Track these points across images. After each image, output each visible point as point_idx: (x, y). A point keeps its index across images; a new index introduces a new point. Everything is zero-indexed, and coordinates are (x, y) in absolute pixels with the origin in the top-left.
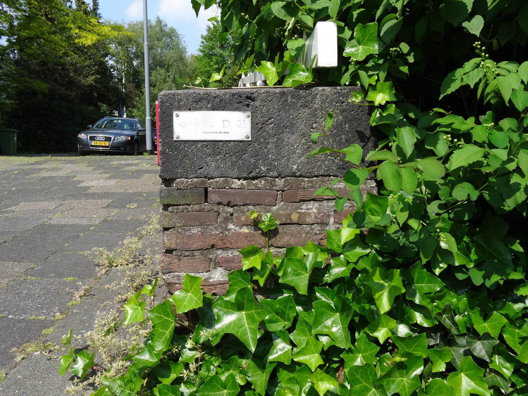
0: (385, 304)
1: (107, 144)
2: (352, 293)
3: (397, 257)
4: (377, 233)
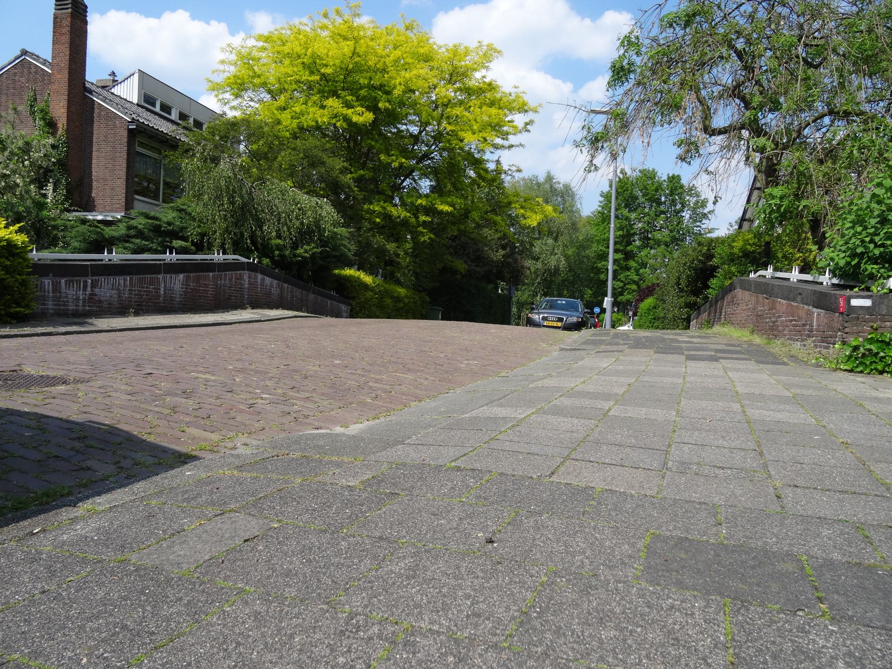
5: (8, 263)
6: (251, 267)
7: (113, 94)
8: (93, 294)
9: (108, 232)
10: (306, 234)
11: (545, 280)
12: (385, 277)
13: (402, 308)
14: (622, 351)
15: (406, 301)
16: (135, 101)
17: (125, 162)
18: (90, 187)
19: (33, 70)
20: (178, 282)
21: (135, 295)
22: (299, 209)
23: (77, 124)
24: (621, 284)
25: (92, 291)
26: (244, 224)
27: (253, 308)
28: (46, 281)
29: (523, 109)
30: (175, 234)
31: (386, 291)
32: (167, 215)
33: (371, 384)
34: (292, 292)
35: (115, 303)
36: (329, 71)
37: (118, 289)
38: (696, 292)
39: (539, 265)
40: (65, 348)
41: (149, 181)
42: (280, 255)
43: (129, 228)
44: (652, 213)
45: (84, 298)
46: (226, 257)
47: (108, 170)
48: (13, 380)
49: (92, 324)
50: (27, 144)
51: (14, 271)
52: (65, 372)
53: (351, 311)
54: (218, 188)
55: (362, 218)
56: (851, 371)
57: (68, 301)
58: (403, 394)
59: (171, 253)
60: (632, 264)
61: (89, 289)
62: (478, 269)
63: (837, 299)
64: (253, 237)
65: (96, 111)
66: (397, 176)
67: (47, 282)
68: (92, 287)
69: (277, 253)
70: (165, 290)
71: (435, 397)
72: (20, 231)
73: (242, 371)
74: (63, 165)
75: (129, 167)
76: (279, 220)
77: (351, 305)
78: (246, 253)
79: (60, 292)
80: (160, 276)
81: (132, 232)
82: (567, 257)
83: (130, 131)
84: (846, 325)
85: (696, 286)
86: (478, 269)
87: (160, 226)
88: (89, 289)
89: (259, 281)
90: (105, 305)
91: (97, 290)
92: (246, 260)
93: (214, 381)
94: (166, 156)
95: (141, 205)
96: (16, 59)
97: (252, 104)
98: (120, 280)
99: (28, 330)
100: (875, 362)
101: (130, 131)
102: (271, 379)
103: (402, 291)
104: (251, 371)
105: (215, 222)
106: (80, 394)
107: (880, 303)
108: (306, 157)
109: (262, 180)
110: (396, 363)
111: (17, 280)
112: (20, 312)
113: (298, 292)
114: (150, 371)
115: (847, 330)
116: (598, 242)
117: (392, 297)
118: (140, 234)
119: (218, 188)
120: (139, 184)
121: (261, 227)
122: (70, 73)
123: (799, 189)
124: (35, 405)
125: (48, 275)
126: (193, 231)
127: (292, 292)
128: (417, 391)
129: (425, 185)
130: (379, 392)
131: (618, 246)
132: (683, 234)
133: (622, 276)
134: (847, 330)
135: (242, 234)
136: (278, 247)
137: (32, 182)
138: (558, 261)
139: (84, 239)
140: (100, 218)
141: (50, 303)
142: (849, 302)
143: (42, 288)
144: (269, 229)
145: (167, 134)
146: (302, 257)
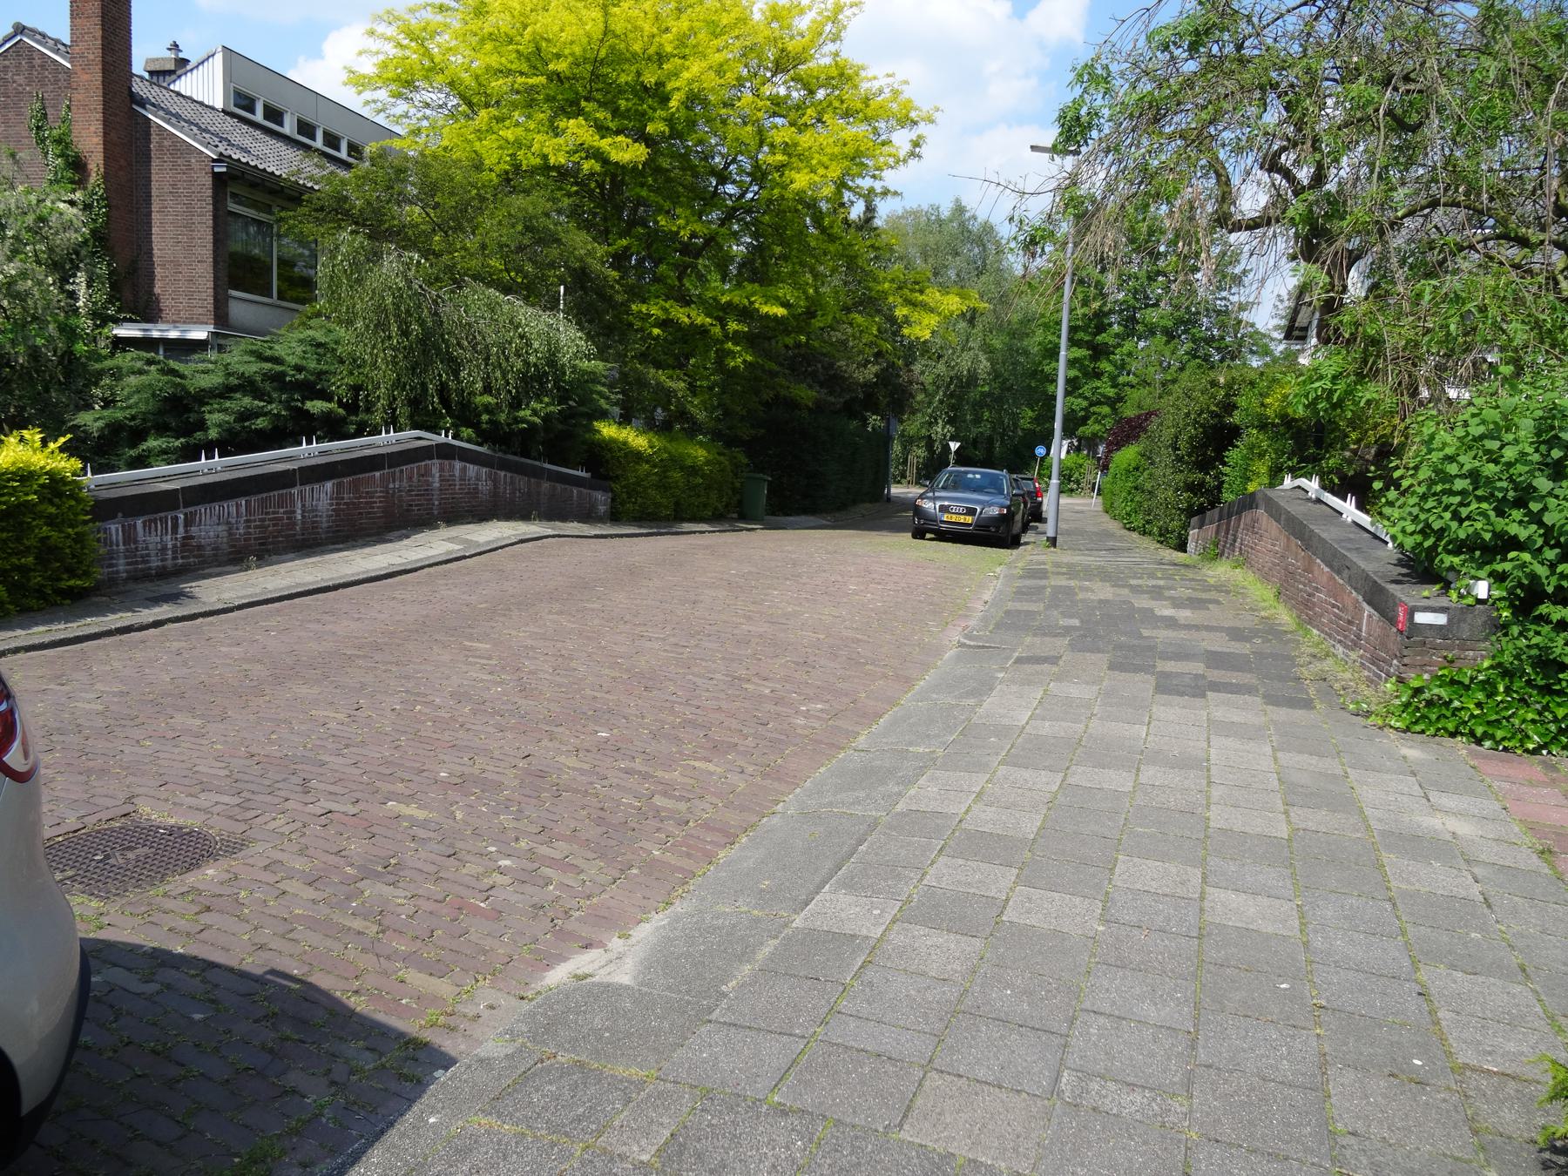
0: (1501, 689)
1: (969, 519)
2: (1489, 687)
3: (1507, 673)
4: (1500, 665)
5: (53, 510)
6: (445, 452)
7: (178, 94)
10: (532, 382)
11: (952, 395)
14: (1054, 660)
16: (219, 105)
17: (210, 232)
19: (37, 62)
20: (323, 497)
22: (522, 337)
23: (122, 162)
24: (1085, 404)
26: (430, 381)
28: (113, 527)
29: (907, 121)
31: (672, 459)
33: (659, 801)
36: (561, 66)
37: (228, 523)
38: (1204, 465)
39: (941, 368)
42: (490, 422)
44: (1143, 274)
45: (175, 546)
47: (181, 246)
53: (613, 500)
56: (1407, 730)
60: (1105, 366)
61: (181, 529)
62: (832, 399)
63: (1395, 605)
64: (443, 390)
65: (154, 138)
67: (115, 528)
68: (186, 526)
76: (487, 359)
79: (136, 542)
80: (295, 491)
81: (234, 381)
82: (988, 349)
83: (217, 177)
84: (1405, 652)
85: (1204, 454)
86: (832, 399)
87: (283, 374)
88: (181, 529)
89: (457, 473)
93: (424, 824)
94: (281, 219)
96: (6, 41)
97: (428, 112)
98: (230, 507)
99: (92, 624)
100: (1445, 717)
101: (217, 177)
103: (698, 453)
107: (1459, 621)
108: (528, 229)
111: (68, 536)
113: (522, 482)
115: (1406, 660)
116: (1046, 326)
117: (682, 468)
119: (380, 309)
121: (456, 373)
122: (104, 71)
123: (1365, 362)
125: (115, 517)
126: (340, 384)
127: (512, 483)
131: (1080, 335)
132: (1198, 313)
133: (1086, 390)
134: (1406, 660)
135: (424, 385)
136: (487, 408)
138: (975, 360)
139: (154, 395)
141: (122, 561)
142: (1412, 617)
143: (107, 542)
144: (472, 377)
146: (527, 422)
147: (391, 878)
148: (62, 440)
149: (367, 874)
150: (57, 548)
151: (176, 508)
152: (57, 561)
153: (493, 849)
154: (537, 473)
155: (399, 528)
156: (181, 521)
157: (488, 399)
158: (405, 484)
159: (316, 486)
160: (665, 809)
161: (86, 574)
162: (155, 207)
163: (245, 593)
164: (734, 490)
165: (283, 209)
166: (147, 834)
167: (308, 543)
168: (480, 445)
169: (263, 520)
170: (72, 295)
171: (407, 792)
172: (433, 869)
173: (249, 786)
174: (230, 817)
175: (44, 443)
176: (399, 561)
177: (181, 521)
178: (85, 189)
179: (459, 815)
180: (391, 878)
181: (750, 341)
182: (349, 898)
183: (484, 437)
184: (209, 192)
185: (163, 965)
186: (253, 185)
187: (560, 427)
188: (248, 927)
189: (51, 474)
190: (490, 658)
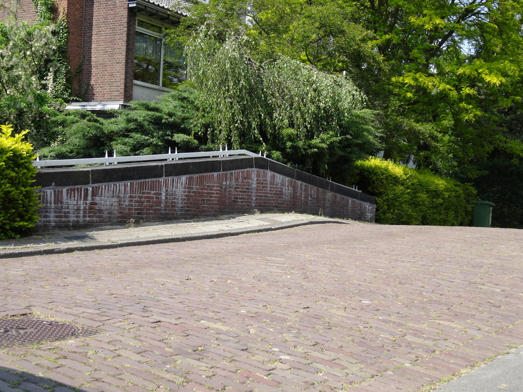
5: (14, 174)
6: (260, 164)
8: (93, 204)
9: (109, 126)
10: (324, 119)
12: (419, 167)
13: (441, 204)
15: (446, 195)
18: (89, 73)
20: (179, 187)
21: (136, 202)
25: (93, 199)
27: (262, 212)
28: (49, 191)
30: (176, 127)
31: (420, 184)
32: (167, 103)
33: (409, 338)
34: (306, 190)
35: (116, 212)
37: (119, 197)
40: (70, 279)
41: (149, 62)
42: (292, 147)
43: (129, 121)
45: (85, 208)
46: (232, 152)
48: (22, 329)
49: (92, 238)
50: (29, 34)
51: (19, 182)
52: (73, 318)
53: (377, 210)
54: (223, 72)
55: (390, 92)
57: (68, 212)
58: (450, 354)
59: (173, 152)
66: (432, 39)
67: (50, 192)
68: (93, 196)
69: (289, 144)
70: (167, 194)
71: (491, 359)
72: (25, 139)
73: (256, 317)
74: (63, 52)
75: (130, 50)
76: (291, 105)
77: (376, 203)
78: (254, 146)
80: (162, 180)
81: (132, 126)
87: (161, 118)
88: (90, 198)
89: (269, 179)
90: (105, 215)
91: (97, 199)
92: (253, 155)
93: (227, 333)
94: (167, 35)
95: (142, 92)
99: (31, 247)
102: (290, 329)
103: (440, 183)
104: (267, 317)
105: (219, 111)
106: (90, 353)
108: (322, 26)
109: (272, 57)
110: (438, 303)
111: (21, 193)
112: (24, 226)
113: (313, 190)
114: (159, 319)
117: (428, 191)
118: (140, 128)
119: (223, 72)
120: (139, 66)
124: (48, 368)
126: (196, 123)
127: (306, 190)
128: (468, 350)
129: (467, 48)
130: (420, 352)
135: (250, 126)
136: (291, 138)
137: (33, 73)
139: (84, 135)
140: (98, 107)
141: (52, 214)
143: (44, 200)
144: (281, 117)
145: (168, 9)
146: (318, 148)
147: (198, 356)
148: (24, 133)
149: (180, 352)
150: (14, 200)
151: (88, 183)
152: (13, 209)
153: (276, 350)
154: (324, 186)
155: (228, 213)
156: (90, 192)
157: (291, 131)
158: (233, 182)
159: (175, 178)
160: (415, 343)
161: (30, 220)
162: (94, 32)
163: (125, 238)
164: (467, 212)
165: (166, 29)
166: (38, 324)
167: (167, 216)
168: (286, 163)
169: (141, 197)
170: (45, 87)
171: (216, 317)
172: (229, 355)
173: (106, 306)
174: (91, 319)
175: (13, 135)
176: (227, 228)
177: (90, 192)
178: (56, 23)
179: (252, 331)
180: (198, 356)
181: (481, 104)
182: (165, 363)
183: (287, 157)
184: (126, 20)
185: (28, 380)
186: (151, 15)
187: (340, 153)
188: (90, 369)
189: (14, 151)
190: (284, 264)
